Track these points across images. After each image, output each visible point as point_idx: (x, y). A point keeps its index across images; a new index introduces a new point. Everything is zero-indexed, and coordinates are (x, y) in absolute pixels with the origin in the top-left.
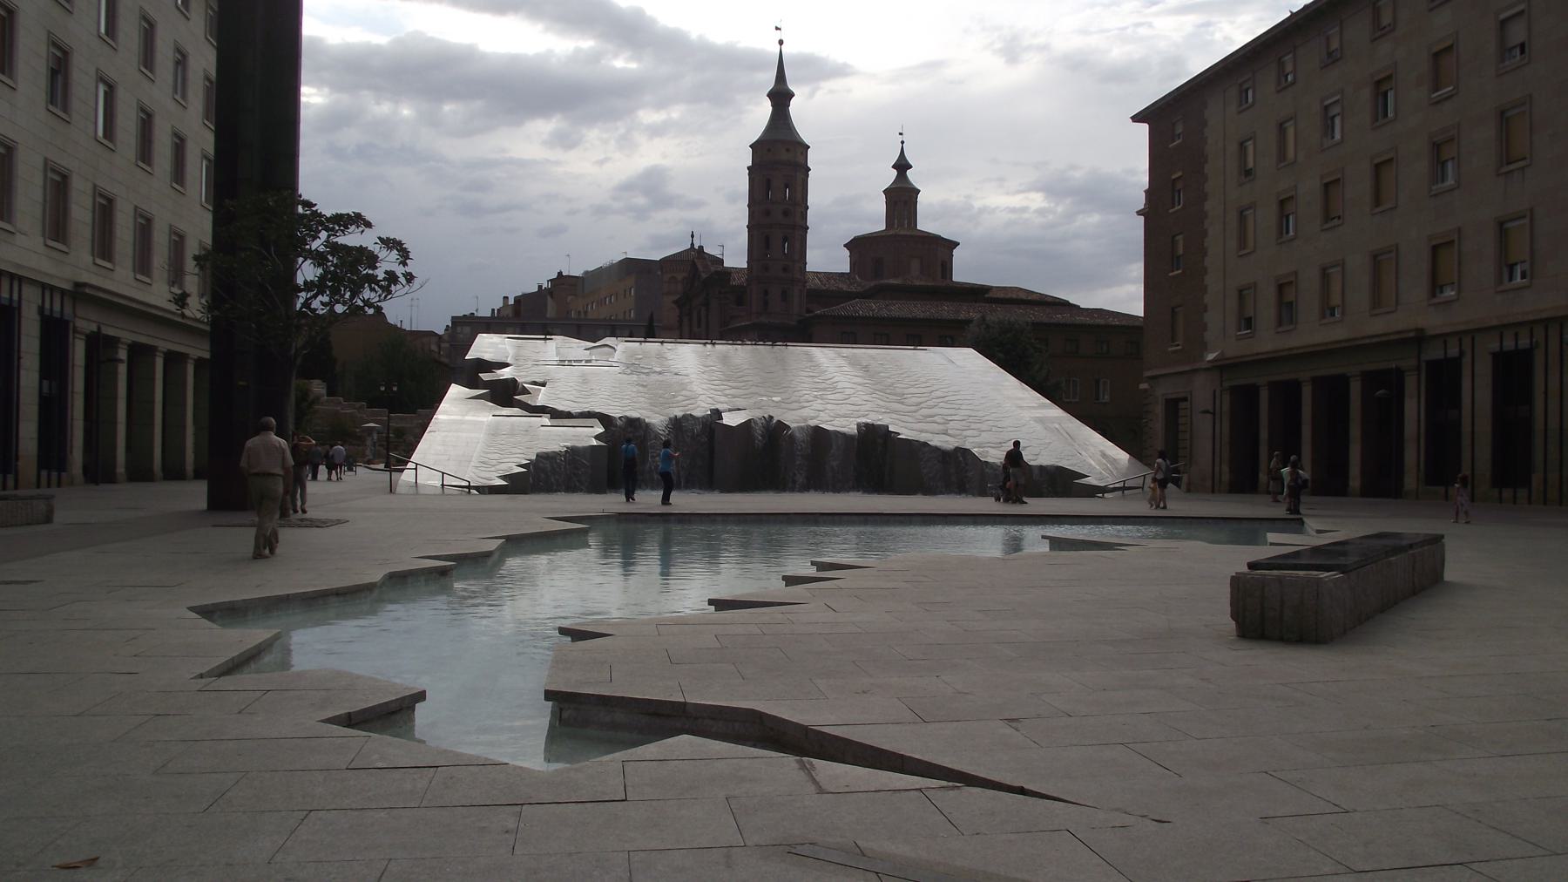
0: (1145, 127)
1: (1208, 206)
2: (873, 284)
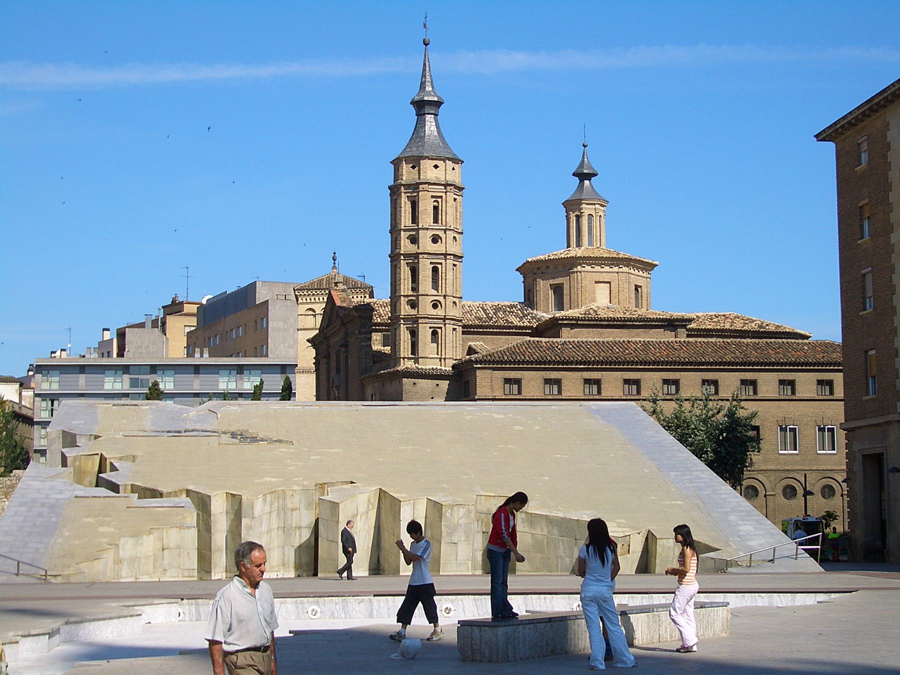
0: (831, 147)
1: (894, 238)
2: (547, 316)
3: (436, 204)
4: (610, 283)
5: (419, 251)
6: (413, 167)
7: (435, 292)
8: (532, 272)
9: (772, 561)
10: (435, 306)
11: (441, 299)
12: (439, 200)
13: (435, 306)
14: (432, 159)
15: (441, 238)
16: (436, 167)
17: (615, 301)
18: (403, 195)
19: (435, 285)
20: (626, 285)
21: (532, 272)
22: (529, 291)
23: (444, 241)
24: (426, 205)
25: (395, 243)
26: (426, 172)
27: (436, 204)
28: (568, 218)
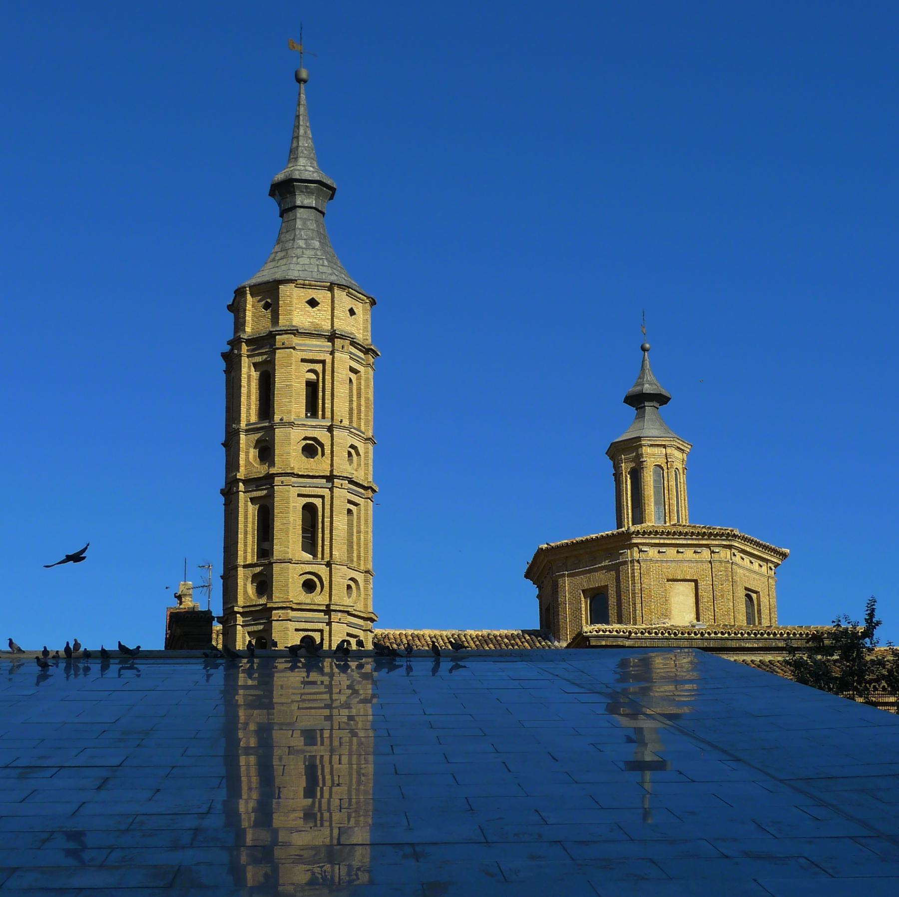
3: (312, 376)
4: (696, 581)
5: (273, 471)
6: (267, 306)
7: (309, 557)
8: (545, 569)
9: (396, 773)
10: (309, 586)
11: (323, 571)
12: (318, 367)
13: (309, 586)
14: (304, 286)
15: (322, 446)
16: (313, 303)
17: (707, 615)
18: (245, 362)
19: (310, 543)
20: (727, 586)
21: (545, 569)
22: (548, 609)
23: (327, 451)
24: (292, 380)
25: (232, 464)
26: (290, 313)
27: (312, 376)
28: (617, 476)
